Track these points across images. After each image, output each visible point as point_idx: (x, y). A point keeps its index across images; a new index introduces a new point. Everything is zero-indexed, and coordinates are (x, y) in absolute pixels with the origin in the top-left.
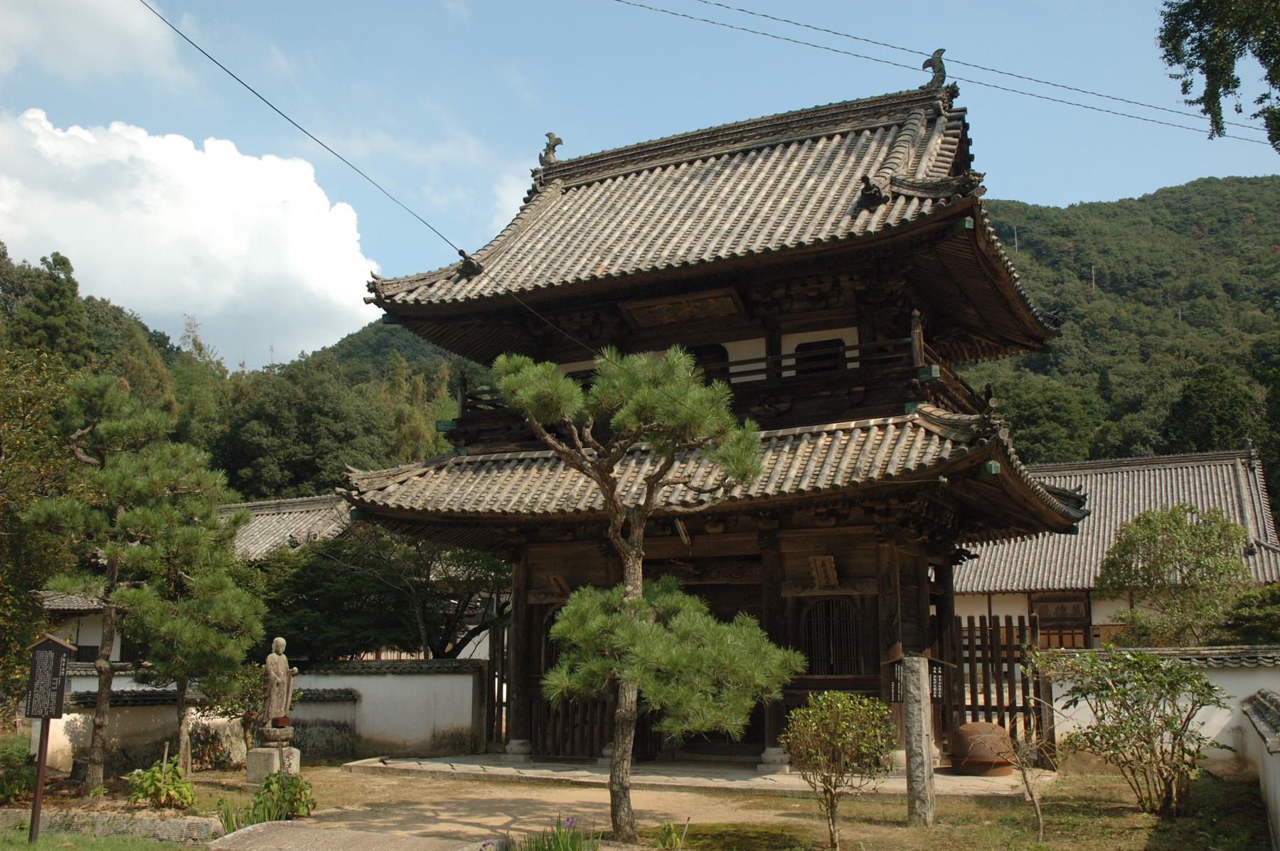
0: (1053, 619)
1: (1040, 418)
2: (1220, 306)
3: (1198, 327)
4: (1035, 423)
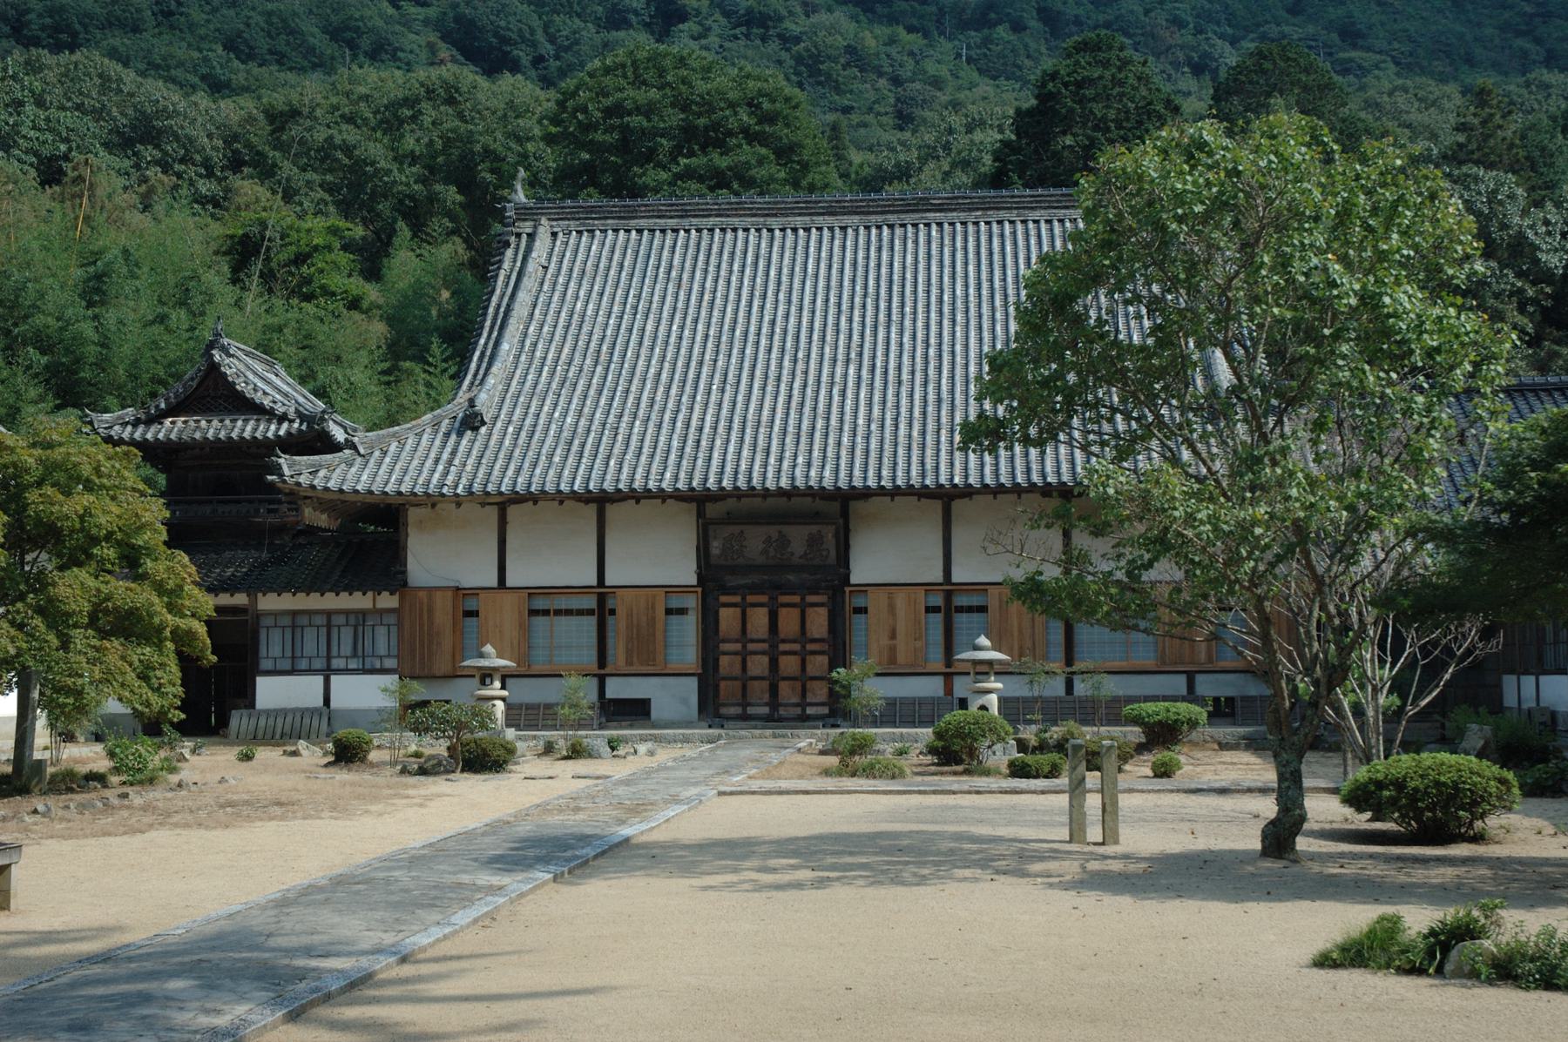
0: (751, 568)
1: (730, 133)
2: (1033, 45)
3: (995, 78)
4: (721, 145)
